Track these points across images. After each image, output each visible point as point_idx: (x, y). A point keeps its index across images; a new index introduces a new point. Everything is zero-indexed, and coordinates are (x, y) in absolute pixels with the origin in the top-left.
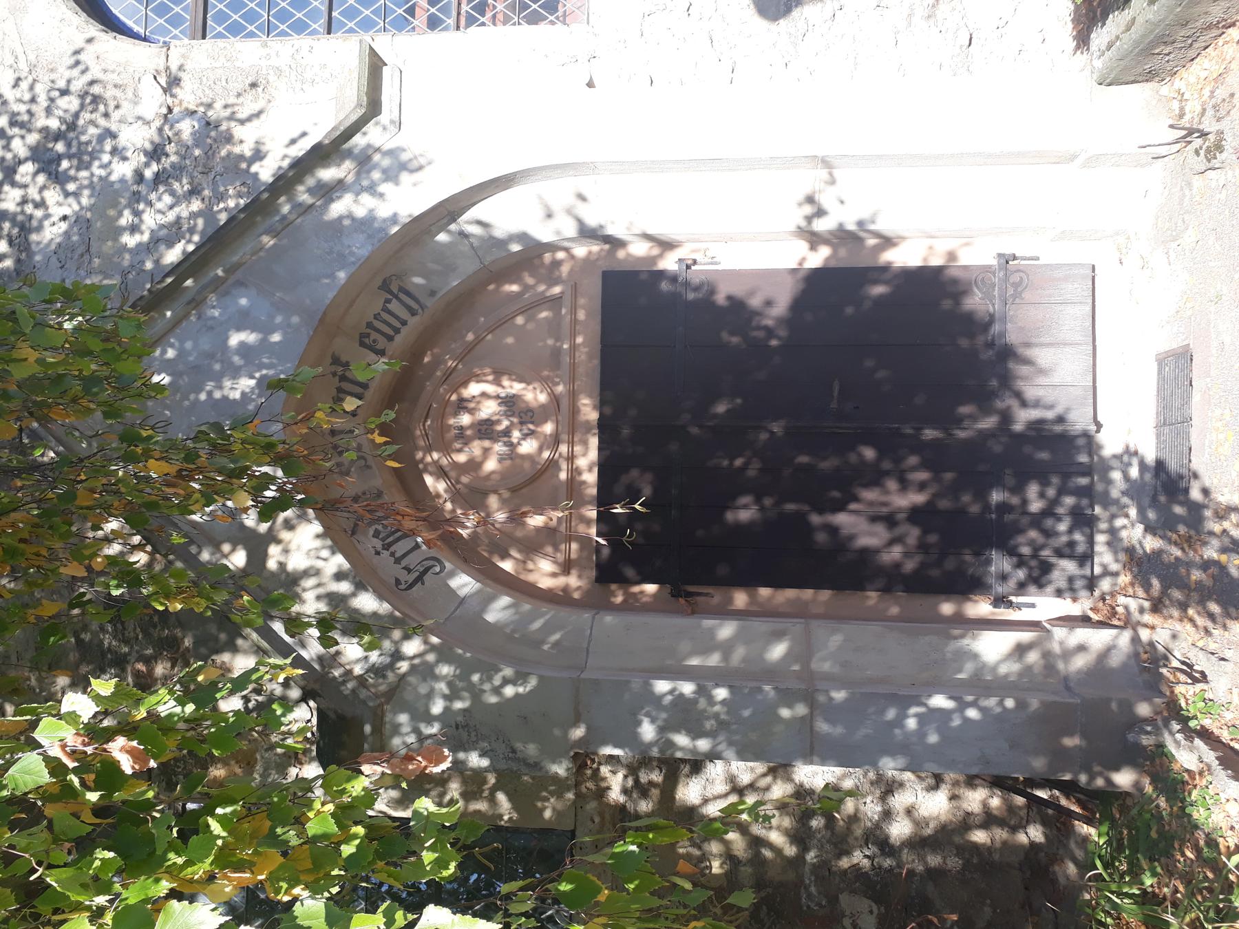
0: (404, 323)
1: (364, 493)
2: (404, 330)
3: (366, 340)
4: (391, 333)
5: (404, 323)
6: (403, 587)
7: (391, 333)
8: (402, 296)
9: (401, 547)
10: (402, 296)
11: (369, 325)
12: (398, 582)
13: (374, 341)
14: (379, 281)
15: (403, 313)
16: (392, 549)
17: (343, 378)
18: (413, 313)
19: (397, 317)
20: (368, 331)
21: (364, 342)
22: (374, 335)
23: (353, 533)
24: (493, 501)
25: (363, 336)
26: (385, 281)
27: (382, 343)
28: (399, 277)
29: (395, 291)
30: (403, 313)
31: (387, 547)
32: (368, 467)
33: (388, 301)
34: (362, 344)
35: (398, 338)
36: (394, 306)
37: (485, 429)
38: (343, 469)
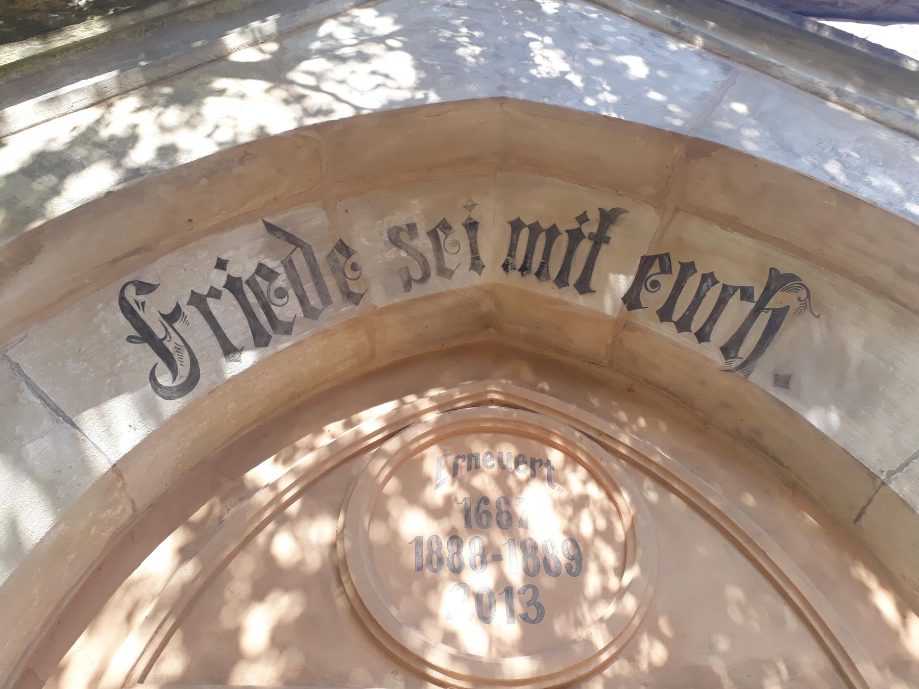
0: (702, 336)
1: (354, 267)
2: (687, 340)
3: (655, 268)
4: (677, 315)
5: (702, 336)
6: (131, 294)
7: (677, 315)
8: (763, 319)
9: (227, 311)
10: (763, 319)
11: (688, 268)
12: (145, 288)
13: (655, 284)
14: (787, 264)
15: (723, 331)
16: (227, 295)
17: (575, 237)
18: (727, 350)
19: (713, 318)
20: (676, 269)
21: (649, 267)
22: (667, 283)
23: (270, 228)
24: (323, 530)
25: (664, 261)
26: (792, 277)
27: (653, 300)
28: (807, 303)
29: (773, 303)
30: (723, 331)
31: (233, 285)
32: (408, 284)
33: (746, 294)
34: (646, 262)
35: (668, 330)
36: (736, 311)
37: (488, 515)
38: (404, 237)
